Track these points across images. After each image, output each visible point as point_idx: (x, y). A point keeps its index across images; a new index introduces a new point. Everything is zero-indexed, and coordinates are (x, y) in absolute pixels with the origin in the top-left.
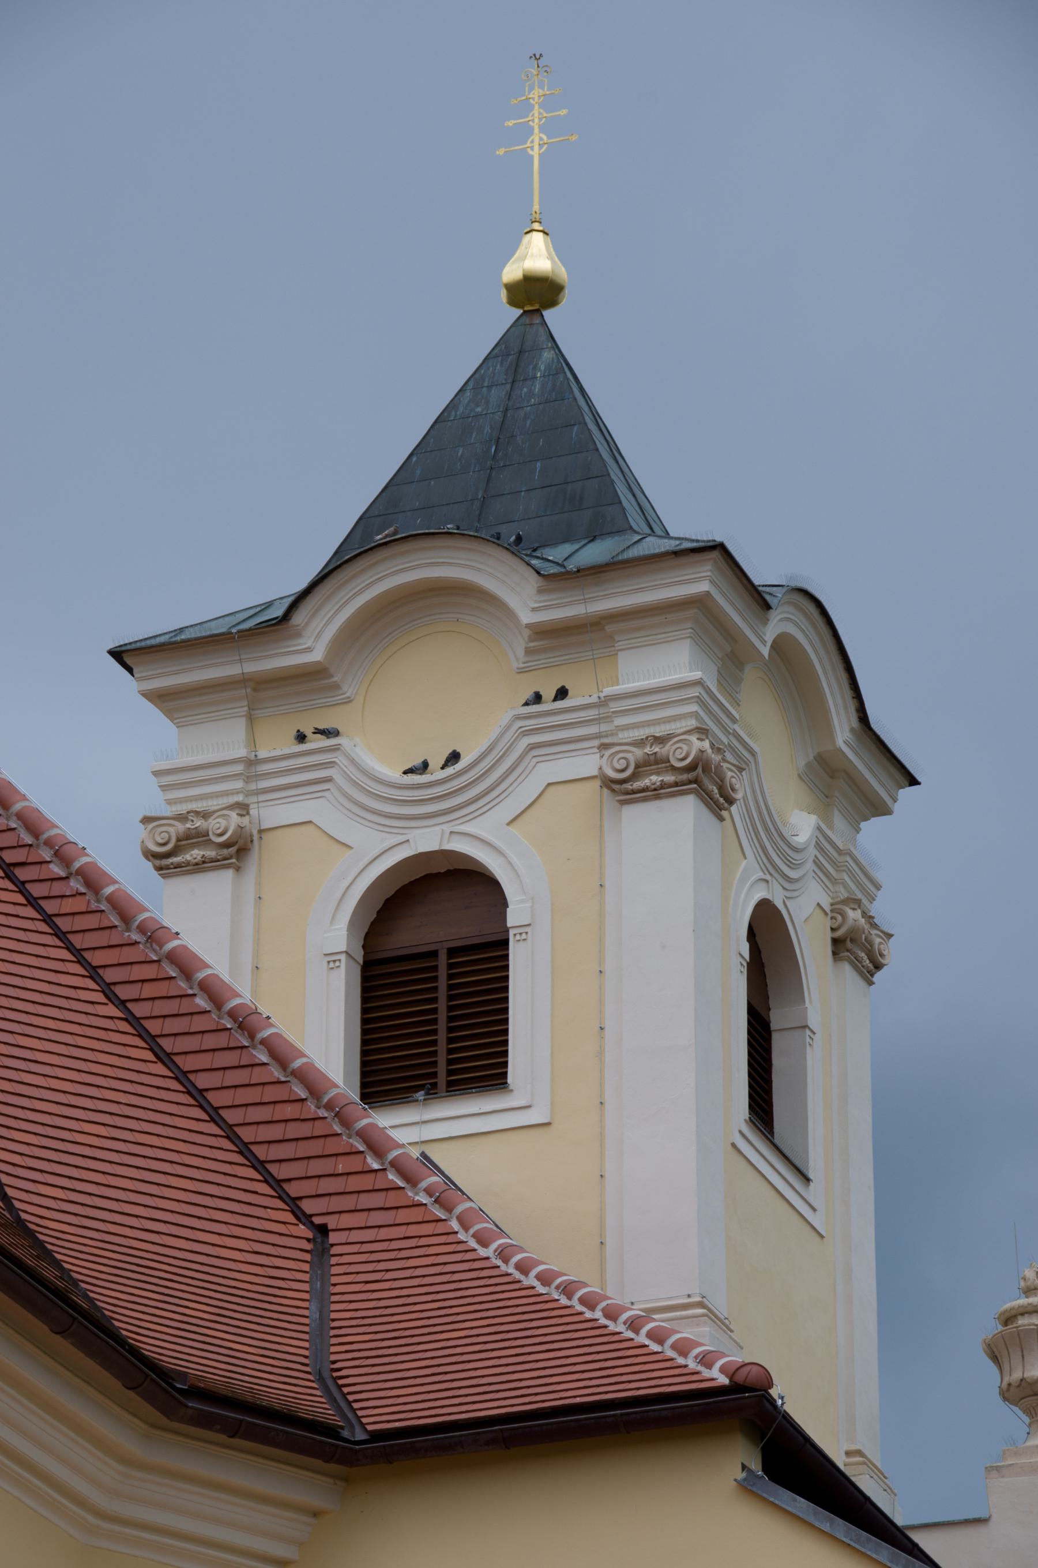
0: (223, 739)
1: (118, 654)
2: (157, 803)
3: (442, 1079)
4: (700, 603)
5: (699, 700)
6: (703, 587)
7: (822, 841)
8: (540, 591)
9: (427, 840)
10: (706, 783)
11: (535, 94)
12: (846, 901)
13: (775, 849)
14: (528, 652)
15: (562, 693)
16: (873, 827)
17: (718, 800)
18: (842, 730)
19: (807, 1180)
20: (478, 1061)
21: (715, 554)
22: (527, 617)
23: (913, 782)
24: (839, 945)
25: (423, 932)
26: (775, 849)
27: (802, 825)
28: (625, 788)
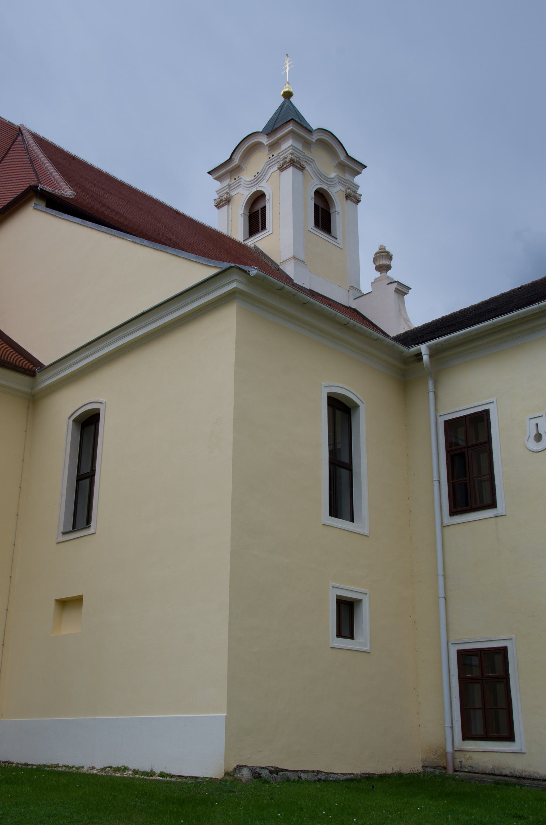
0: (227, 182)
1: (209, 173)
4: (292, 131)
5: (292, 149)
6: (291, 128)
7: (339, 178)
8: (267, 138)
9: (254, 190)
10: (294, 163)
11: (287, 61)
12: (347, 188)
14: (269, 151)
15: (273, 156)
18: (342, 157)
19: (336, 239)
21: (292, 121)
22: (266, 144)
23: (366, 167)
24: (348, 197)
28: (282, 169)
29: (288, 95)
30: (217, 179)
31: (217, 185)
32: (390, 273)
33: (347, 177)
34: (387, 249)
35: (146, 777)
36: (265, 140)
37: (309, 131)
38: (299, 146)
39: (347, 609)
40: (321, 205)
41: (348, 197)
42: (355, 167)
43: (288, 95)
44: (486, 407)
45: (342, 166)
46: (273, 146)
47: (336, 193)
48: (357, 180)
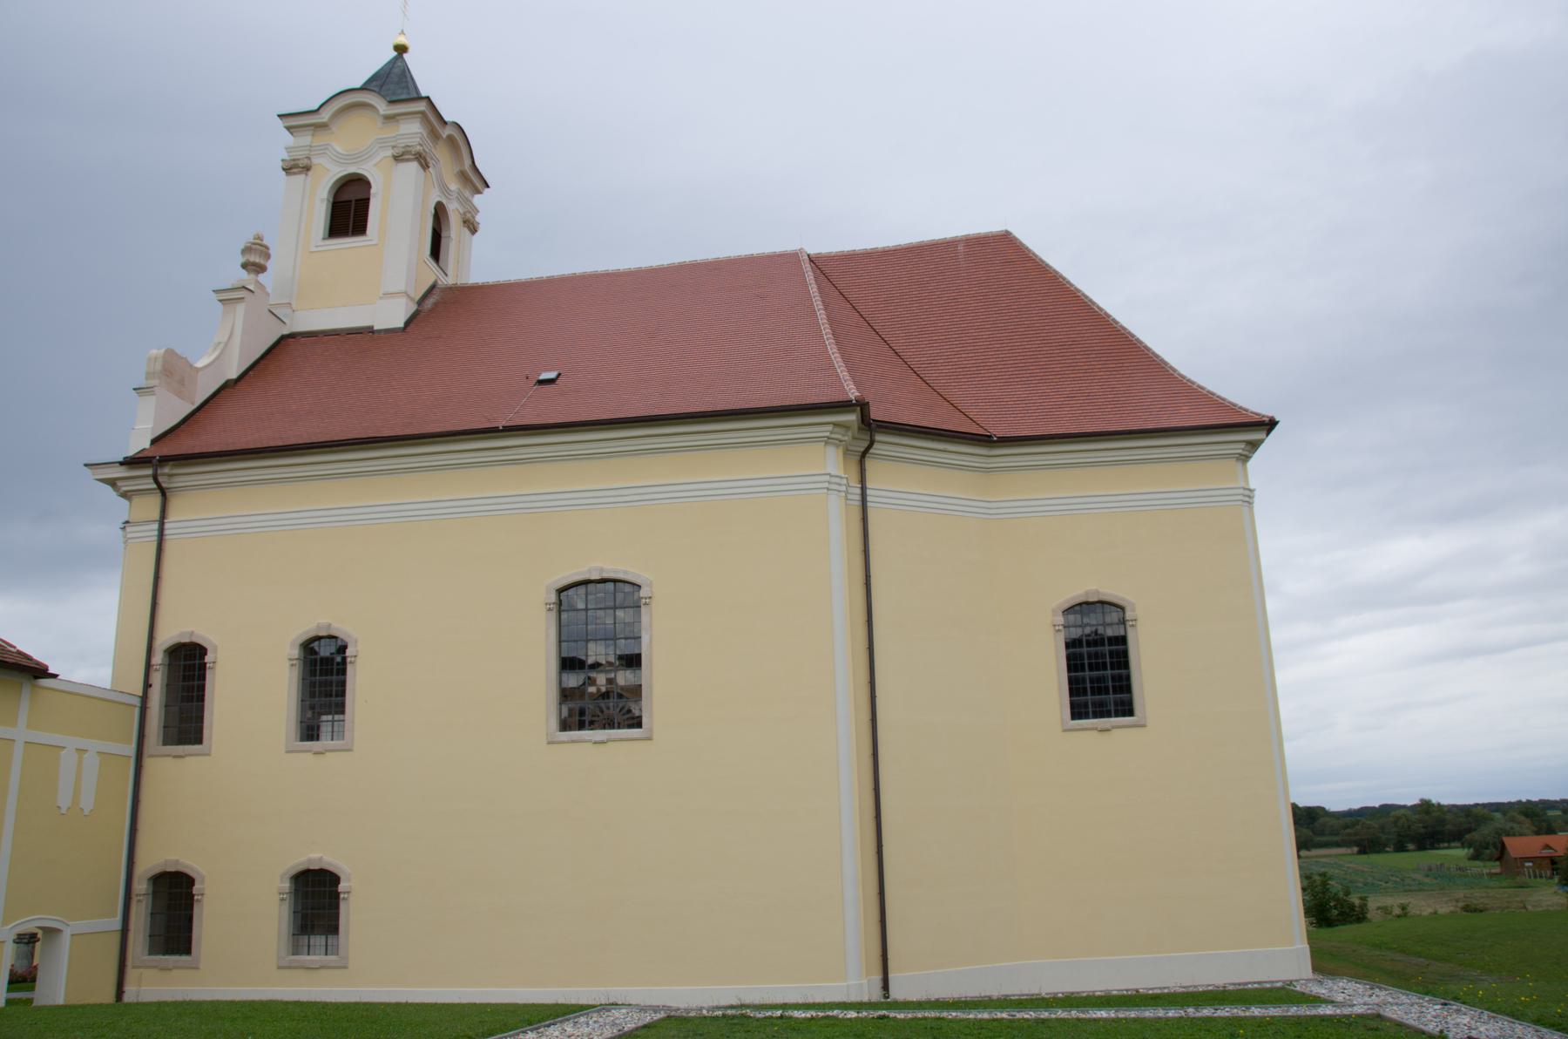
0: (305, 139)
2: (286, 157)
3: (1123, 672)
4: (422, 113)
9: (352, 170)
10: (423, 161)
13: (444, 189)
16: (477, 197)
17: (425, 166)
18: (467, 163)
20: (359, 228)
25: (352, 195)
26: (444, 189)
27: (454, 186)
28: (398, 158)
29: (401, 49)
30: (288, 128)
31: (288, 139)
32: (262, 277)
33: (467, 194)
34: (265, 242)
35: (1045, 1015)
39: (598, 690)
43: (401, 49)
45: (463, 176)
46: (389, 118)
47: (454, 209)
48: (477, 200)
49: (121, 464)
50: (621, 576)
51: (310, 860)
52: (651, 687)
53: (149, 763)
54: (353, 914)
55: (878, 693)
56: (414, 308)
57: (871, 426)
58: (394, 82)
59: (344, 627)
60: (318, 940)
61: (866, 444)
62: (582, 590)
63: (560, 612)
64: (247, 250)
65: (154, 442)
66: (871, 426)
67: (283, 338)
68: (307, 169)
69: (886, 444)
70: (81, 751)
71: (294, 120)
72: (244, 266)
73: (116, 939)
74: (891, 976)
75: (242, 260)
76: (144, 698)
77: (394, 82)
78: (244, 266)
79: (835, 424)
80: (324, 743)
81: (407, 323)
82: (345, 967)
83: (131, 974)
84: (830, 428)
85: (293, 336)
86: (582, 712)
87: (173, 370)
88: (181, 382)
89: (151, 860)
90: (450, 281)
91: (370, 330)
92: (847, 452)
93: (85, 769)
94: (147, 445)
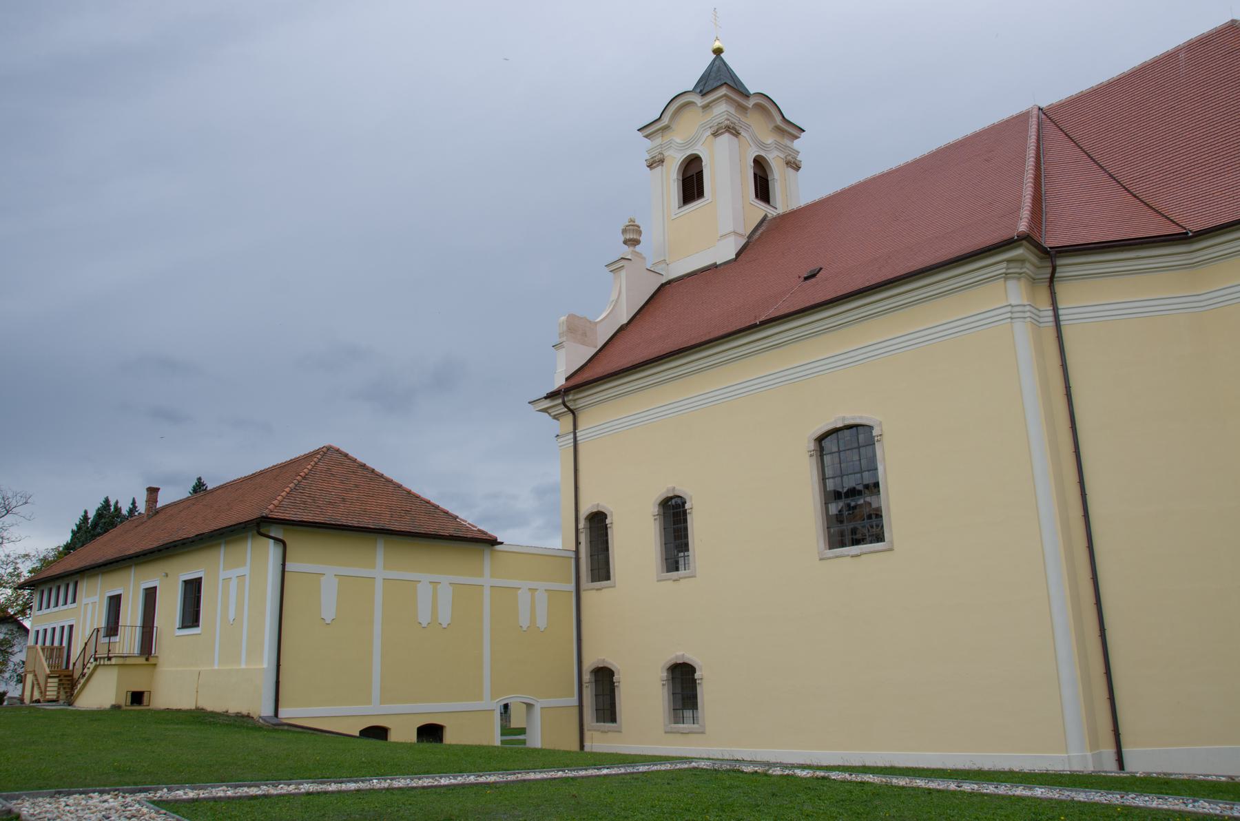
0: (658, 141)
4: (725, 95)
7: (777, 143)
9: (689, 152)
10: (733, 130)
17: (736, 134)
18: (778, 119)
27: (770, 140)
28: (715, 134)
29: (718, 52)
30: (646, 137)
32: (638, 248)
33: (787, 142)
36: (699, 101)
37: (746, 95)
38: (732, 110)
39: (853, 515)
40: (759, 173)
41: (788, 163)
42: (789, 130)
44: (587, 677)
45: (778, 129)
46: (706, 107)
48: (797, 144)
49: (546, 398)
50: (858, 421)
51: (677, 657)
52: (888, 508)
53: (584, 595)
54: (706, 693)
55: (1087, 492)
56: (743, 241)
57: (1051, 255)
58: (719, 79)
59: (683, 489)
60: (688, 713)
61: (1049, 270)
62: (834, 436)
63: (822, 456)
64: (624, 231)
65: (567, 379)
66: (1051, 255)
67: (663, 285)
68: (662, 161)
69: (1068, 267)
70: (532, 590)
71: (649, 130)
72: (625, 242)
73: (576, 711)
74: (1124, 750)
75: (622, 239)
76: (577, 552)
77: (719, 79)
78: (625, 242)
79: (1009, 261)
80: (681, 573)
81: (738, 255)
82: (703, 733)
83: (587, 734)
84: (1004, 265)
85: (669, 282)
86: (854, 531)
87: (576, 328)
88: (584, 334)
89: (590, 663)
90: (781, 209)
91: (715, 266)
92: (1033, 281)
93: (538, 603)
94: (563, 382)
